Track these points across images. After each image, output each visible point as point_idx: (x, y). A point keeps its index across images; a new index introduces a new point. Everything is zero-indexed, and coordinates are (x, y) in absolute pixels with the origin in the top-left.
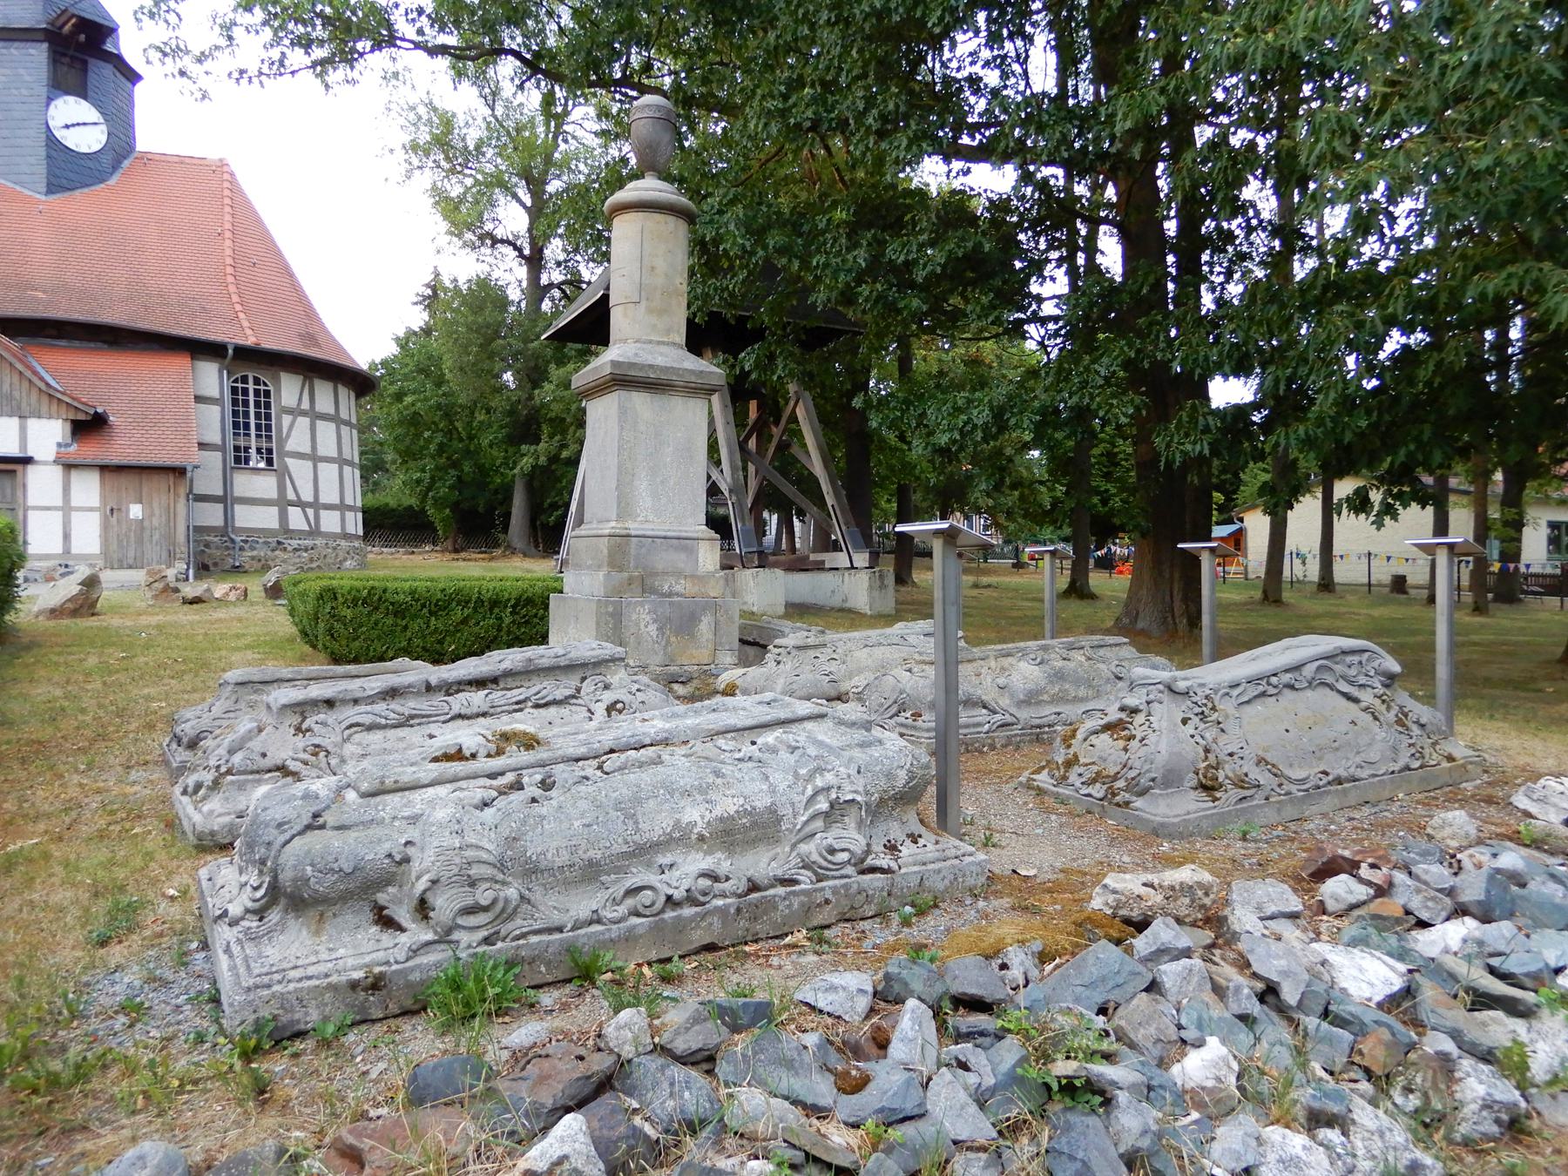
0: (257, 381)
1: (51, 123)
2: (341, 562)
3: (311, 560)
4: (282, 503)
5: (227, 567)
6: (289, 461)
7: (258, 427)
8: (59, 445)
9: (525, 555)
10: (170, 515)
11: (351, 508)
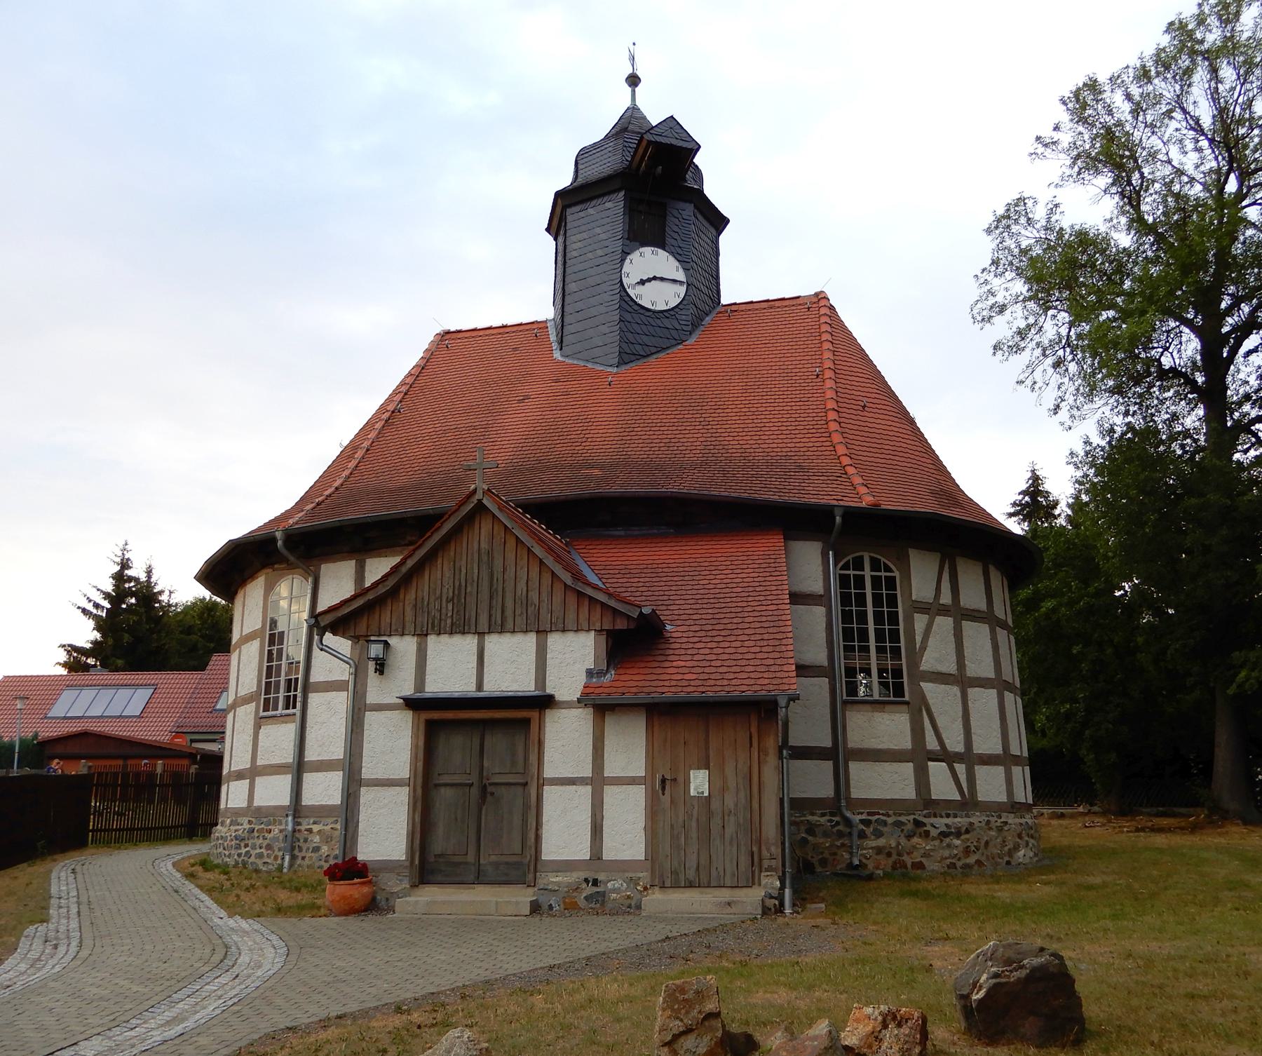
0: (875, 565)
1: (625, 281)
2: (1010, 853)
3: (967, 851)
4: (920, 757)
5: (840, 867)
6: (926, 686)
7: (880, 636)
8: (590, 673)
9: (1246, 822)
10: (753, 784)
11: (1017, 760)
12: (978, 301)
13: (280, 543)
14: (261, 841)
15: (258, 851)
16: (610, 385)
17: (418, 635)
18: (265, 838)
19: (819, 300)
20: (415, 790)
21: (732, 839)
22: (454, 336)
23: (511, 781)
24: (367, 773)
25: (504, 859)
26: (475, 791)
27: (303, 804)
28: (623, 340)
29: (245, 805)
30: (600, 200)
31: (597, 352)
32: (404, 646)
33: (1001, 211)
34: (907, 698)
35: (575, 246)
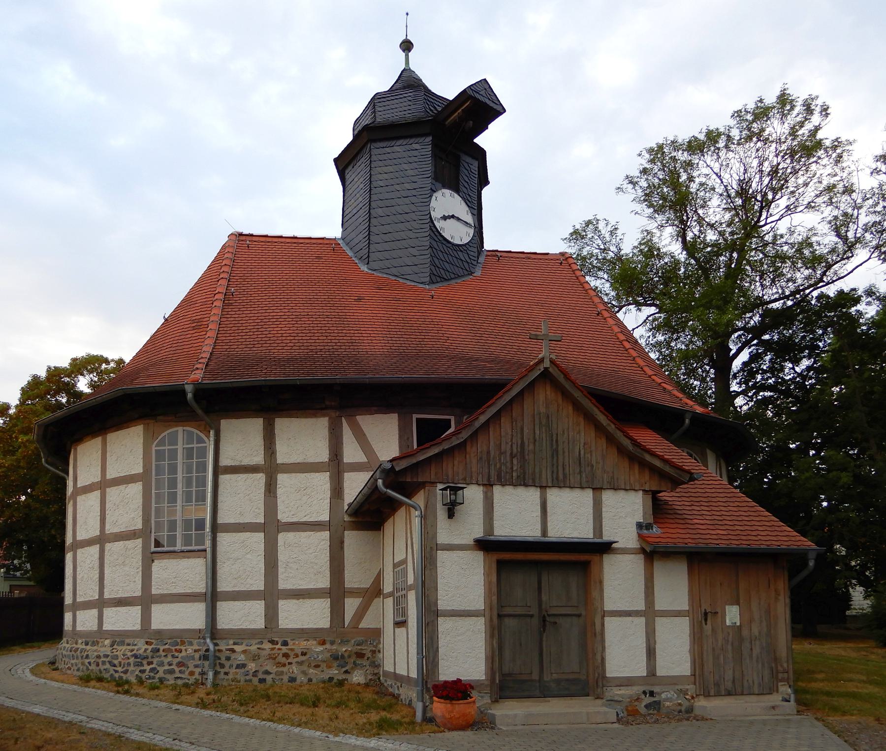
8: (639, 526)
13: (190, 396)
14: (169, 659)
15: (167, 667)
17: (484, 485)
20: (491, 620)
21: (758, 658)
23: (569, 612)
24: (443, 604)
25: (565, 677)
26: (535, 621)
32: (473, 494)
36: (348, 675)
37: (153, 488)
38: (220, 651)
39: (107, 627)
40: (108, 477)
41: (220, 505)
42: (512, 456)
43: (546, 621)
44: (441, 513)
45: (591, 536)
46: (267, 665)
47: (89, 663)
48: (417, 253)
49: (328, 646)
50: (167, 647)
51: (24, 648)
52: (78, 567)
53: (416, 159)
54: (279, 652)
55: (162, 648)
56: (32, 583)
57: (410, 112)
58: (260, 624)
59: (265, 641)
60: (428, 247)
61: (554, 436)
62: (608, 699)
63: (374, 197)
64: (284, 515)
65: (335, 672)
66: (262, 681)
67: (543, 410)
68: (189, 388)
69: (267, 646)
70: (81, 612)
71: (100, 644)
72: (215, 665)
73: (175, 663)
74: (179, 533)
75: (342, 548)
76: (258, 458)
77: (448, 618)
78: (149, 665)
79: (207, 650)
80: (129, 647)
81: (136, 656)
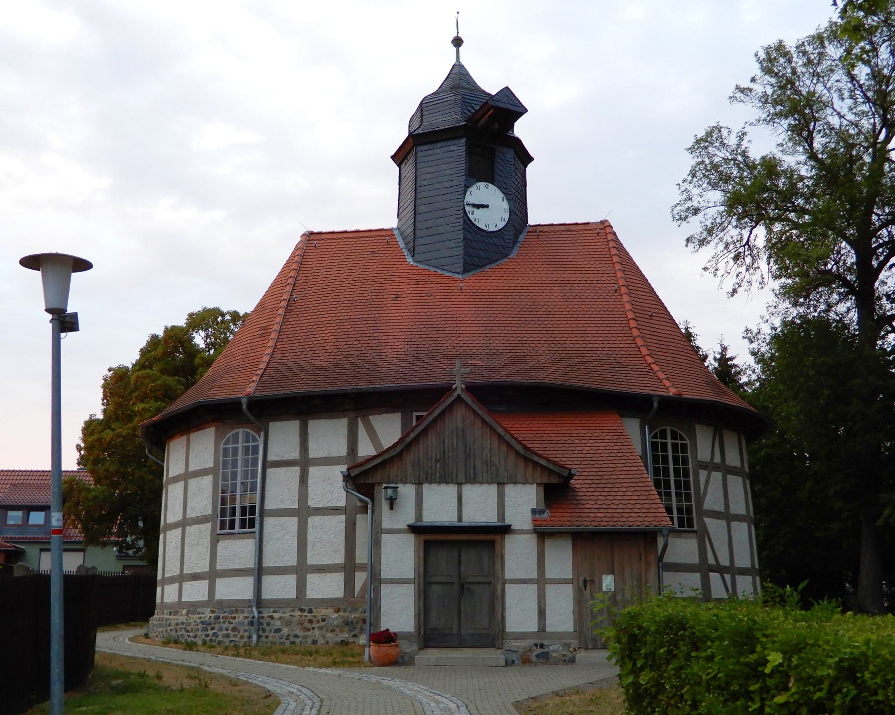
0: (674, 436)
4: (704, 568)
6: (707, 520)
8: (534, 511)
12: (678, 204)
13: (244, 406)
14: (227, 625)
15: (225, 632)
16: (461, 290)
17: (416, 483)
18: (230, 623)
19: (605, 227)
20: (419, 586)
22: (318, 237)
24: (384, 575)
27: (263, 598)
28: (467, 254)
29: (206, 598)
30: (445, 143)
31: (443, 261)
32: (407, 491)
33: (701, 134)
34: (696, 528)
35: (424, 177)
36: (356, 638)
37: (220, 481)
38: (263, 617)
39: (185, 598)
40: (190, 470)
41: (267, 494)
42: (436, 461)
43: (463, 588)
44: (385, 505)
45: (496, 521)
46: (296, 630)
47: (171, 630)
48: (453, 246)
49: (341, 613)
50: (226, 614)
51: (128, 627)
52: (167, 547)
53: (453, 159)
54: (305, 618)
55: (222, 616)
56: (144, 563)
57: (450, 114)
58: (292, 595)
59: (296, 609)
60: (461, 240)
61: (468, 444)
62: (507, 649)
63: (419, 196)
64: (313, 503)
65: (345, 636)
66: (293, 643)
67: (460, 425)
68: (244, 401)
69: (298, 613)
70: (168, 586)
71: (180, 614)
72: (259, 630)
73: (230, 628)
74: (238, 518)
75: (355, 529)
76: (295, 455)
77: (388, 585)
78: (212, 630)
79: (253, 617)
80: (199, 616)
81: (203, 623)
